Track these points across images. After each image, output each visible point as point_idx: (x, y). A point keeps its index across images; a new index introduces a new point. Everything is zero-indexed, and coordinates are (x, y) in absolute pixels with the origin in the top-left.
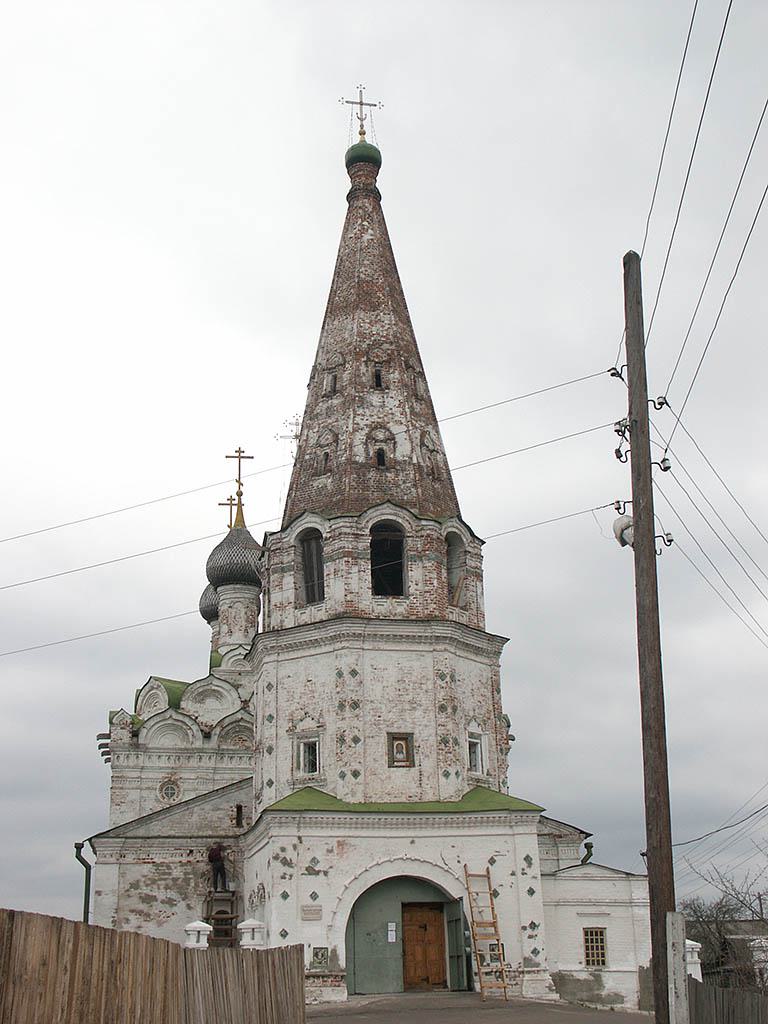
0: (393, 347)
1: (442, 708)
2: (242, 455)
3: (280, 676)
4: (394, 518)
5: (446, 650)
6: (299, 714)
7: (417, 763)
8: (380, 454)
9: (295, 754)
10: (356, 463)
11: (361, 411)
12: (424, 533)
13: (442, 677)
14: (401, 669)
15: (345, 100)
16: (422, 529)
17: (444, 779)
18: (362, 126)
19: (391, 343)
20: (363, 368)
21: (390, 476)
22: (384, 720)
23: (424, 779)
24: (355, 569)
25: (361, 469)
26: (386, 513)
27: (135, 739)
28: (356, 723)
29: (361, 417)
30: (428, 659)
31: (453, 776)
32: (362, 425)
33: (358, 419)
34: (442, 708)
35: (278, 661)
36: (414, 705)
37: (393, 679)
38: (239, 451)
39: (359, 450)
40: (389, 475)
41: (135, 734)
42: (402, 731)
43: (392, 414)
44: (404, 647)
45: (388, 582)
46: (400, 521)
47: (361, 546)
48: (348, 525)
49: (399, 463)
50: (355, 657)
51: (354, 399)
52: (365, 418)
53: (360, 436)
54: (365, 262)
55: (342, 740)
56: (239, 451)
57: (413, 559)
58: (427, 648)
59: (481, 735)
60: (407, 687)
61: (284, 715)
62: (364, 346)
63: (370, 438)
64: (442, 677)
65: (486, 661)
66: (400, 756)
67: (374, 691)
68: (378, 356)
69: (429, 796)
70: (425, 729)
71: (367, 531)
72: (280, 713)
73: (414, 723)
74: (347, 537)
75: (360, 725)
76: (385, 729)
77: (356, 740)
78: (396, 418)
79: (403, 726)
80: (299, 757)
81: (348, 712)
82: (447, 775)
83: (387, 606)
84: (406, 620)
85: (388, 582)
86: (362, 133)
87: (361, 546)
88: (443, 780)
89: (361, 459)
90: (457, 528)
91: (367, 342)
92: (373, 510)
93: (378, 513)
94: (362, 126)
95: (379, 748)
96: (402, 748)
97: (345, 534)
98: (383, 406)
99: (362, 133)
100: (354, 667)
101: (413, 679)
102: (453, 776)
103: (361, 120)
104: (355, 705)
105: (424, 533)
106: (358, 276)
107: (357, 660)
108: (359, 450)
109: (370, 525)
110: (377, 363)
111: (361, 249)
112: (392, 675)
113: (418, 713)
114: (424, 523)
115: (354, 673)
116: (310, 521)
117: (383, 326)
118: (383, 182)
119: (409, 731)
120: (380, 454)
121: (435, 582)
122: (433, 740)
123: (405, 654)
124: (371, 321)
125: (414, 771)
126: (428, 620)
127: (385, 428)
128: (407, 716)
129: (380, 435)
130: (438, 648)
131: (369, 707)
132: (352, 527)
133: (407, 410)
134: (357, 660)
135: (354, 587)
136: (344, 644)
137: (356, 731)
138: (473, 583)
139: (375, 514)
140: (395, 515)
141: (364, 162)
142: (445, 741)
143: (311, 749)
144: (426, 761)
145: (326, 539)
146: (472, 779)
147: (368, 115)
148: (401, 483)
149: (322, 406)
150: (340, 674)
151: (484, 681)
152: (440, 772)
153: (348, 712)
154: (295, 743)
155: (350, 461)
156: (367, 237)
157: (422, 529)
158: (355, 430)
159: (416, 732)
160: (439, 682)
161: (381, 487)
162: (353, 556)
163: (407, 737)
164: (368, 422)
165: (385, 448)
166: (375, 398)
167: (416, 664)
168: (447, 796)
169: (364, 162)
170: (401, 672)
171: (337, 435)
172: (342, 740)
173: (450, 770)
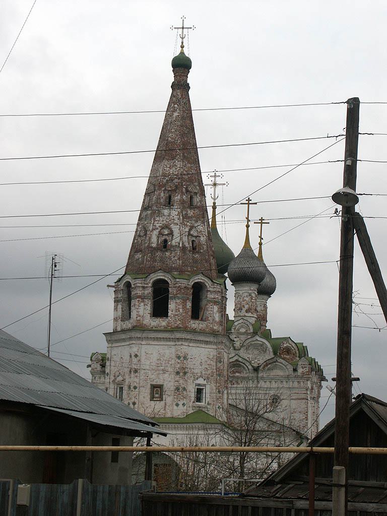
0: (180, 181)
1: (178, 373)
2: (263, 221)
3: (112, 354)
4: (163, 278)
5: (182, 345)
6: (117, 374)
7: (164, 399)
8: (166, 241)
9: (115, 392)
10: (152, 247)
11: (158, 219)
12: (177, 285)
13: (179, 357)
14: (160, 354)
15: (192, 29)
16: (176, 283)
17: (176, 407)
18: (182, 43)
19: (179, 179)
20: (162, 194)
21: (168, 254)
22: (150, 379)
23: (167, 407)
24: (142, 304)
25: (153, 250)
26: (160, 275)
27: (103, 368)
28: (137, 380)
29: (157, 222)
30: (173, 350)
31: (181, 406)
32: (157, 227)
33: (156, 222)
34: (178, 373)
35: (111, 347)
36: (164, 371)
37: (155, 359)
38: (262, 219)
39: (154, 239)
40: (167, 253)
41: (103, 366)
42: (158, 383)
43: (174, 219)
44: (162, 343)
45: (160, 310)
46: (166, 279)
47: (146, 292)
48: (140, 282)
49: (173, 246)
50: (137, 348)
51: (155, 212)
52: (159, 222)
53: (156, 233)
54: (173, 130)
55: (129, 387)
56: (262, 219)
57: (172, 298)
58: (173, 343)
59: (206, 385)
60: (162, 362)
61: (112, 373)
62: (165, 181)
63: (160, 234)
64: (179, 357)
65: (215, 347)
66: (157, 395)
67: (146, 363)
68: (171, 187)
69: (169, 415)
70: (169, 382)
71: (150, 285)
72: (111, 372)
73: (164, 380)
74: (144, 287)
75: (137, 380)
76: (149, 383)
77: (135, 388)
78: (175, 222)
79: (159, 381)
80: (117, 393)
81: (132, 375)
82: (177, 405)
83: (162, 322)
84: (165, 331)
85: (160, 310)
86: (182, 47)
87: (146, 292)
88: (175, 407)
89: (154, 245)
90: (201, 279)
91: (167, 179)
92: (153, 274)
93: (156, 275)
94: (182, 43)
95: (146, 393)
96: (157, 391)
97: (138, 287)
98: (169, 215)
99: (182, 47)
100: (136, 353)
101: (165, 358)
102: (181, 406)
103: (182, 38)
104: (136, 371)
105: (177, 285)
106: (167, 140)
107: (138, 350)
108: (154, 239)
109: (151, 281)
110: (170, 191)
111: (171, 123)
112: (155, 356)
113: (166, 375)
114: (177, 280)
115: (136, 356)
116: (128, 278)
117: (176, 169)
118: (191, 79)
119: (161, 383)
120: (166, 241)
121: (181, 310)
122: (173, 388)
123: (162, 347)
124: (170, 166)
125: (162, 403)
126: (177, 329)
127: (168, 228)
128: (161, 377)
129: (166, 232)
130: (178, 343)
131: (143, 372)
132: (141, 283)
133: (181, 217)
134: (138, 350)
135: (141, 313)
136: (134, 342)
137: (136, 383)
138: (211, 307)
139: (154, 276)
140: (164, 276)
141: (181, 65)
142: (177, 389)
143: (121, 389)
144: (169, 399)
145: (133, 288)
146: (194, 407)
147: (186, 36)
148: (172, 257)
149: (144, 214)
150: (131, 356)
151: (211, 357)
152: (174, 403)
153: (132, 375)
154: (116, 387)
155: (149, 247)
156: (176, 114)
157: (176, 283)
158: (153, 230)
159: (165, 384)
160: (177, 360)
161: (162, 260)
162: (142, 298)
163: (160, 387)
164: (161, 225)
165: (168, 238)
166: (166, 212)
167: (167, 351)
168: (177, 415)
169: (181, 65)
170: (159, 355)
171: (146, 231)
172: (129, 387)
173: (179, 403)
